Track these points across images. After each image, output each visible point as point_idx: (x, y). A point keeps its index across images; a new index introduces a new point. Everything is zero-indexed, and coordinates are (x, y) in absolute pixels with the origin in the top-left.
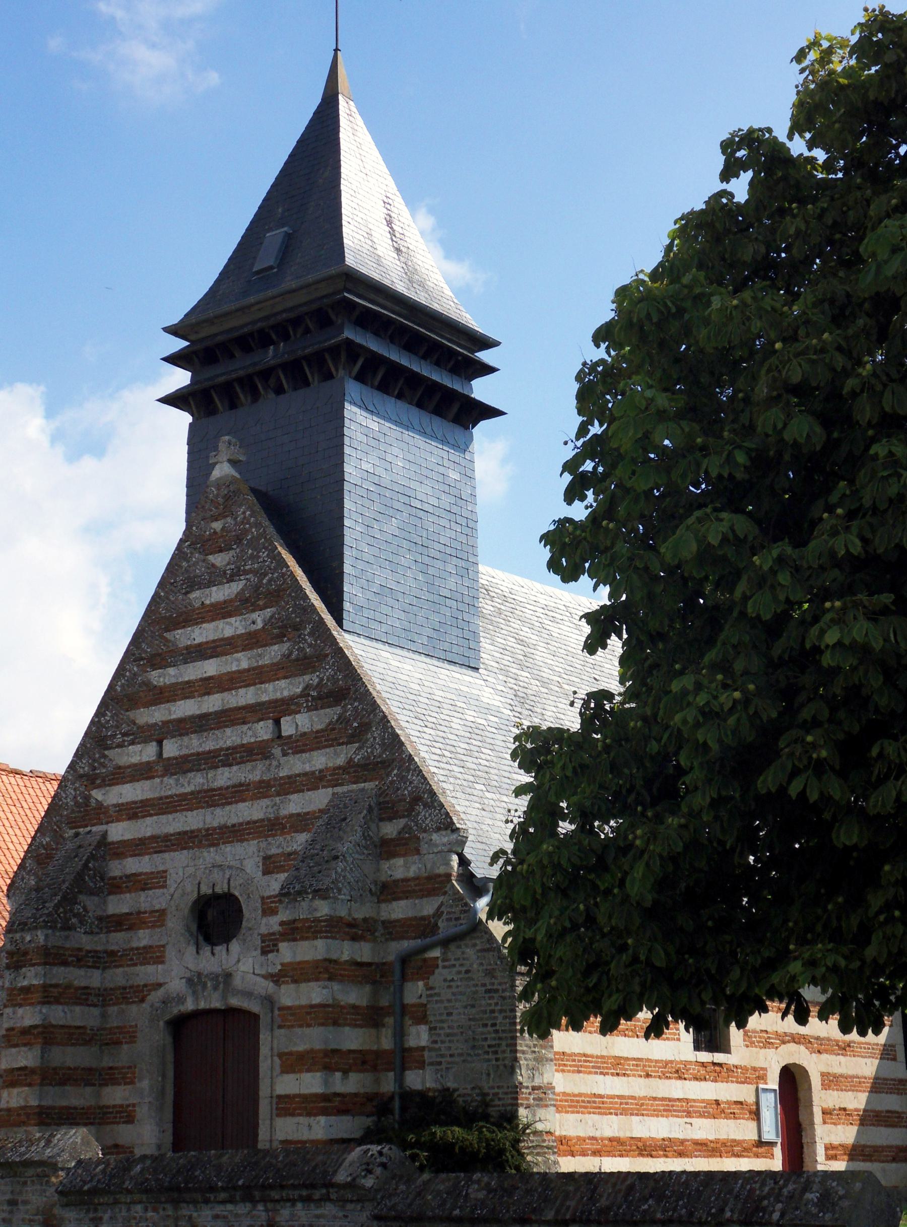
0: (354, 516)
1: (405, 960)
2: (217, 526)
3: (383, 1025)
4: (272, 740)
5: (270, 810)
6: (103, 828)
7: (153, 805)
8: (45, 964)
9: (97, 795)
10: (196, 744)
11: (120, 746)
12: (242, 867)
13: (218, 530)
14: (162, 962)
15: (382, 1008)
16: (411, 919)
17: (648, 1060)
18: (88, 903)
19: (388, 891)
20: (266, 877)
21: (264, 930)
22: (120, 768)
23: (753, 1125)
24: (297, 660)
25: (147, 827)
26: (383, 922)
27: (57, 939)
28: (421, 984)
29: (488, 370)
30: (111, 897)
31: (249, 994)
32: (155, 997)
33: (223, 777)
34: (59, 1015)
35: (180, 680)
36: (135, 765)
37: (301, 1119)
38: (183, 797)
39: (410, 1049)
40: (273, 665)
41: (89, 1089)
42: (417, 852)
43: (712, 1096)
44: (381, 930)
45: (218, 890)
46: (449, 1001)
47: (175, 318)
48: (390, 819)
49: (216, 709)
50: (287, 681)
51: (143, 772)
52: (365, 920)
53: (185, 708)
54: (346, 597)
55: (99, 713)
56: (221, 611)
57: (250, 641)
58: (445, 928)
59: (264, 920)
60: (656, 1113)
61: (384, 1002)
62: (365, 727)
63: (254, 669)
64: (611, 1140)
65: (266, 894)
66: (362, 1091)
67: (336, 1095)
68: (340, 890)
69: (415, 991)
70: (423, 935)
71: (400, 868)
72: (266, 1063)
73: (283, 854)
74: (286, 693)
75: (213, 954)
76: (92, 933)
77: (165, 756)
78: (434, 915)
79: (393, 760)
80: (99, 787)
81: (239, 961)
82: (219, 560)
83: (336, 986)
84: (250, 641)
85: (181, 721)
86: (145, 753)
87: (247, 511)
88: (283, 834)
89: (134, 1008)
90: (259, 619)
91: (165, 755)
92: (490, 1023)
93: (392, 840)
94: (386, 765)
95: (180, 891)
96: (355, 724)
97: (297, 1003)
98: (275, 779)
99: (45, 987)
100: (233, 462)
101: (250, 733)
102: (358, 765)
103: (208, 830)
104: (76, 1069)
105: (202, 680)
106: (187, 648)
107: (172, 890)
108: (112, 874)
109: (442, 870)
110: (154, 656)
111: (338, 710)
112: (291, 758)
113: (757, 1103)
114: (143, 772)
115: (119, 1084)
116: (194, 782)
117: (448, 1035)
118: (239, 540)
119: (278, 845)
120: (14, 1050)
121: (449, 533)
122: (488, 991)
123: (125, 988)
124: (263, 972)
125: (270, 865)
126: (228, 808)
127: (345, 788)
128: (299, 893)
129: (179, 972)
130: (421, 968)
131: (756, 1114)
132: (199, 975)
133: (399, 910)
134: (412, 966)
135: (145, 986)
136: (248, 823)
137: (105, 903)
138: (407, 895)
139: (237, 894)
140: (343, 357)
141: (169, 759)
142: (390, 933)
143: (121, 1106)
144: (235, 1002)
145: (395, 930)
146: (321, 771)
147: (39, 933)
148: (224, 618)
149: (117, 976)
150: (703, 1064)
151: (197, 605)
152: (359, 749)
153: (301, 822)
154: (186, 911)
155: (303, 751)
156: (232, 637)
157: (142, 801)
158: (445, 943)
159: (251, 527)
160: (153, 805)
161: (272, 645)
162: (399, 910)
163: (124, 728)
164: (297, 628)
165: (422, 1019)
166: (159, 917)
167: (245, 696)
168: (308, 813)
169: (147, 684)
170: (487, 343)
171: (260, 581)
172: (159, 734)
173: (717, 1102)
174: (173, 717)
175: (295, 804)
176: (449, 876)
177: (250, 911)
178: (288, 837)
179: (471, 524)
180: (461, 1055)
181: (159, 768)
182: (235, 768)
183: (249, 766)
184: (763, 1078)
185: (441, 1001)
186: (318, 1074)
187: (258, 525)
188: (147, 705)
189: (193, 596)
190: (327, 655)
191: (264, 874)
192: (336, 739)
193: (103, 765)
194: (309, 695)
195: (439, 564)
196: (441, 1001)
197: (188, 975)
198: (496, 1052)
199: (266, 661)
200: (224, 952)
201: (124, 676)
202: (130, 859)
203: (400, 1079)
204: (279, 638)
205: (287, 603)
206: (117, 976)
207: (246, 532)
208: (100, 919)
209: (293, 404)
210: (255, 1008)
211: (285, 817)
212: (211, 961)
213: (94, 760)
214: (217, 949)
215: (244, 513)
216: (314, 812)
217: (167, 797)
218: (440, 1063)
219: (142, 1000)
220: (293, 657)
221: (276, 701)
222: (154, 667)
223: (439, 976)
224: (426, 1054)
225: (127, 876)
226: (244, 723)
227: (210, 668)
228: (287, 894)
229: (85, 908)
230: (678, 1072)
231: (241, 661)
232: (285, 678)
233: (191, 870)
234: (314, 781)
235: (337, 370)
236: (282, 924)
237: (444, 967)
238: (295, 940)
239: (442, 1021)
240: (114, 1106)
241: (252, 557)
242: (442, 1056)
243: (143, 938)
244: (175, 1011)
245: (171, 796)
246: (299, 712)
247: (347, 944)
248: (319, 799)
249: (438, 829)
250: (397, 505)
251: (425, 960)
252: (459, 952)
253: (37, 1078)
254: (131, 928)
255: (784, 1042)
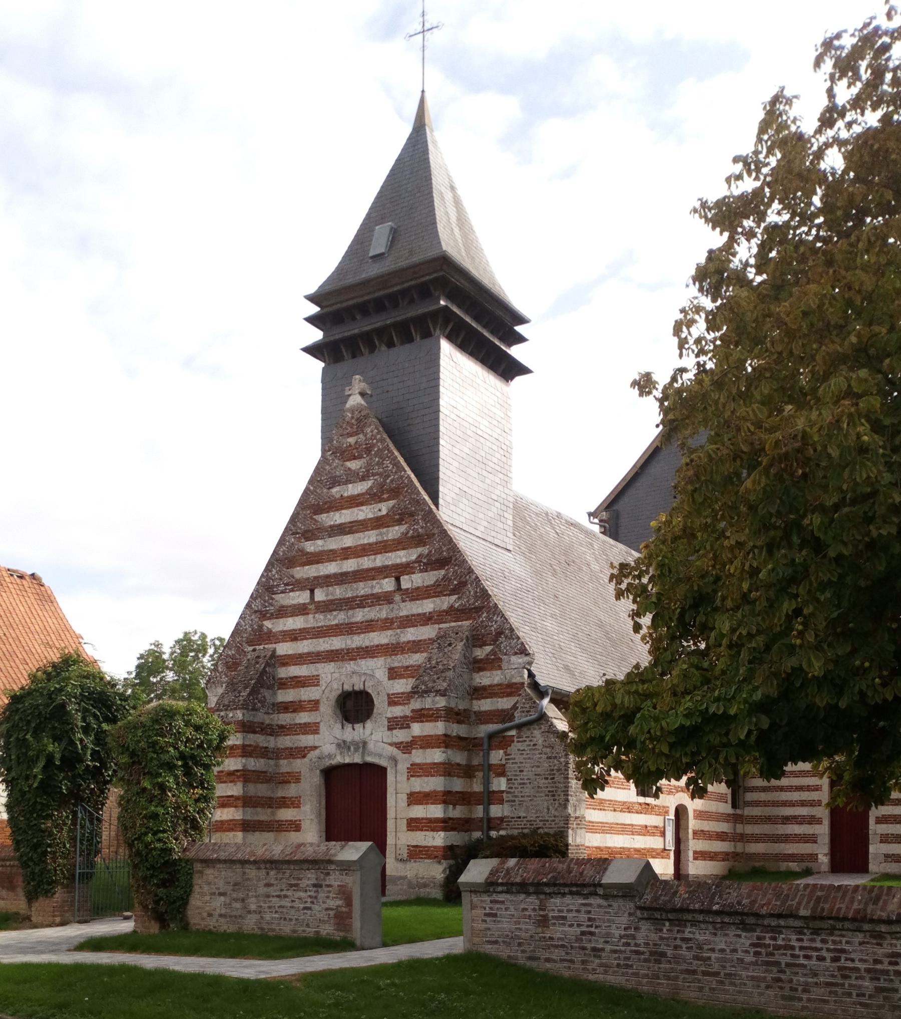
0: (446, 438)
1: (491, 736)
2: (352, 440)
3: (475, 777)
4: (394, 591)
5: (393, 638)
6: (274, 646)
7: (308, 632)
8: (243, 732)
9: (268, 624)
10: (338, 592)
11: (282, 592)
12: (373, 674)
13: (353, 443)
14: (318, 733)
15: (474, 766)
16: (494, 711)
17: (616, 801)
18: (266, 694)
19: (479, 692)
20: (391, 682)
21: (389, 715)
22: (283, 607)
23: (661, 839)
24: (412, 537)
25: (304, 647)
26: (475, 712)
27: (249, 717)
28: (501, 752)
29: (521, 339)
30: (280, 691)
31: (380, 756)
32: (313, 755)
33: (359, 615)
34: (253, 764)
35: (326, 549)
36: (295, 605)
37: (427, 833)
38: (330, 628)
39: (493, 791)
40: (394, 540)
41: (270, 810)
42: (500, 668)
43: (643, 823)
44: (473, 717)
45: (356, 688)
46: (521, 763)
47: (312, 289)
48: (481, 646)
49: (352, 569)
50: (405, 551)
51: (301, 610)
52: (465, 710)
53: (332, 568)
54: (441, 495)
55: (267, 569)
56: (355, 502)
57: (378, 523)
58: (519, 718)
59: (390, 708)
60: (618, 833)
61: (475, 762)
62: (463, 584)
63: (381, 542)
64: (596, 848)
65: (391, 692)
66: (463, 816)
67: (450, 819)
68: (452, 691)
69: (496, 757)
70: (503, 721)
71: (485, 679)
72: (872, 821)
73: (402, 667)
74: (404, 560)
75: (354, 729)
76: (269, 713)
77: (316, 600)
78: (511, 709)
79: (483, 607)
80: (269, 619)
81: (372, 734)
82: (354, 465)
83: (450, 752)
84: (378, 523)
85: (327, 577)
86: (302, 597)
87: (372, 429)
88: (402, 654)
89: (299, 761)
90: (384, 508)
91: (316, 600)
92: (550, 777)
93: (481, 660)
94: (478, 610)
95: (329, 688)
96: (455, 582)
97: (424, 762)
98: (397, 618)
99: (244, 746)
100: (362, 394)
101: (378, 586)
102: (457, 610)
103: (348, 650)
104: (262, 797)
105: (343, 549)
106: (331, 527)
107: (323, 688)
108: (280, 676)
109: (517, 680)
110: (306, 531)
111: (443, 572)
112: (408, 604)
113: (664, 827)
114: (301, 610)
115: (290, 808)
116: (338, 618)
117: (520, 784)
118: (368, 450)
119: (400, 661)
120: (223, 785)
121: (499, 456)
122: (549, 758)
123: (291, 749)
124: (390, 741)
125: (393, 674)
126: (363, 635)
127: (447, 625)
128: (426, 692)
129: (330, 740)
130: (501, 742)
131: (663, 834)
132: (344, 742)
133: (485, 705)
134: (498, 740)
135: (306, 747)
136: (377, 646)
137: (275, 694)
138: (492, 695)
139: (370, 691)
140: (440, 321)
141: (319, 602)
142: (480, 720)
143: (291, 821)
144: (369, 759)
145: (484, 717)
146: (430, 613)
147: (238, 711)
148: (357, 506)
149: (286, 741)
150: (640, 804)
151: (338, 496)
152: (459, 598)
153: (416, 646)
154: (334, 700)
155: (417, 599)
156: (364, 520)
157: (300, 630)
158: (519, 727)
159: (377, 442)
160: (308, 632)
161: (393, 526)
162: (485, 705)
163: (286, 580)
164: (412, 515)
165: (502, 774)
166: (315, 705)
167: (379, 561)
168: (420, 641)
169: (302, 551)
170: (522, 320)
171: (385, 481)
172: (311, 585)
173: (646, 827)
174: (322, 573)
175: (411, 634)
176: (523, 684)
177: (380, 702)
178: (406, 656)
179: (509, 450)
180: (529, 796)
181: (312, 607)
182: (367, 609)
183: (378, 608)
184: (667, 812)
185: (516, 763)
186: (439, 806)
187: (382, 440)
188: (304, 564)
189: (334, 490)
190: (434, 534)
191: (389, 679)
192: (441, 592)
193: (271, 604)
194: (421, 562)
195: (491, 476)
196: (516, 763)
197: (336, 741)
198: (554, 796)
199: (390, 536)
200: (361, 729)
201: (284, 545)
202: (293, 667)
203: (487, 811)
204: (399, 522)
205: (405, 497)
206: (286, 741)
207: (374, 445)
208: (273, 704)
209: (401, 354)
210: (383, 763)
211: (404, 643)
212: (352, 733)
213: (265, 601)
214: (356, 726)
215: (372, 431)
216: (425, 640)
217: (318, 627)
218: (514, 801)
219: (304, 757)
220: (409, 535)
221: (397, 565)
222: (307, 539)
223: (515, 747)
224: (504, 795)
225: (291, 678)
226: (373, 579)
227: (348, 541)
228: (414, 693)
229: (264, 697)
230: (628, 808)
231: (370, 537)
232: (404, 549)
233: (336, 675)
234: (426, 619)
235: (435, 330)
236: (413, 711)
237: (518, 742)
238: (422, 722)
239: (516, 775)
240: (286, 821)
241: (378, 464)
242: (516, 796)
243: (303, 718)
244: (328, 764)
245: (322, 627)
246: (414, 573)
247: (455, 725)
248: (427, 632)
249: (516, 654)
250: (469, 433)
251: (504, 737)
252: (529, 733)
253: (240, 803)
254: (294, 711)
255: (677, 792)
